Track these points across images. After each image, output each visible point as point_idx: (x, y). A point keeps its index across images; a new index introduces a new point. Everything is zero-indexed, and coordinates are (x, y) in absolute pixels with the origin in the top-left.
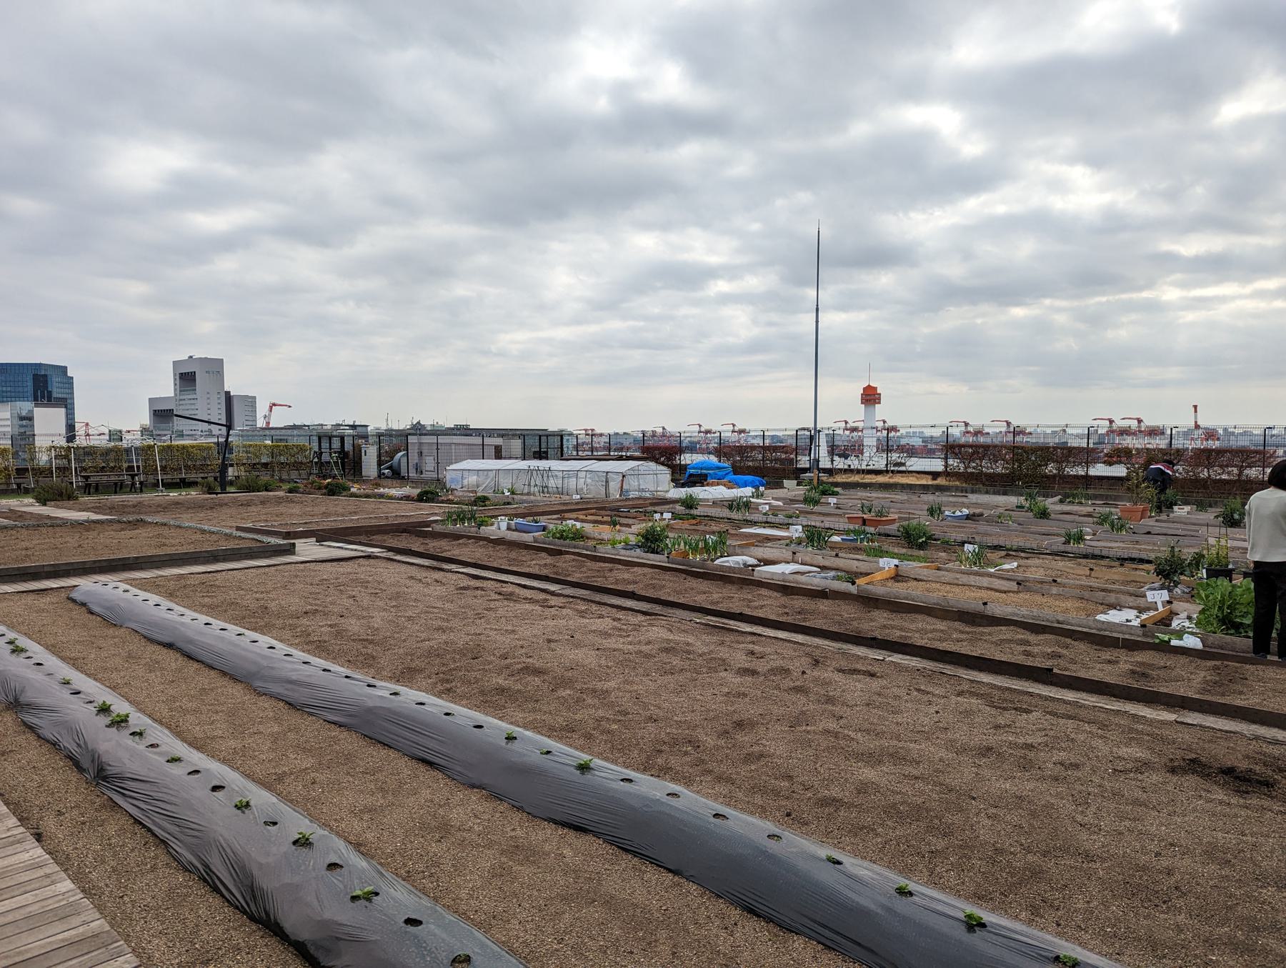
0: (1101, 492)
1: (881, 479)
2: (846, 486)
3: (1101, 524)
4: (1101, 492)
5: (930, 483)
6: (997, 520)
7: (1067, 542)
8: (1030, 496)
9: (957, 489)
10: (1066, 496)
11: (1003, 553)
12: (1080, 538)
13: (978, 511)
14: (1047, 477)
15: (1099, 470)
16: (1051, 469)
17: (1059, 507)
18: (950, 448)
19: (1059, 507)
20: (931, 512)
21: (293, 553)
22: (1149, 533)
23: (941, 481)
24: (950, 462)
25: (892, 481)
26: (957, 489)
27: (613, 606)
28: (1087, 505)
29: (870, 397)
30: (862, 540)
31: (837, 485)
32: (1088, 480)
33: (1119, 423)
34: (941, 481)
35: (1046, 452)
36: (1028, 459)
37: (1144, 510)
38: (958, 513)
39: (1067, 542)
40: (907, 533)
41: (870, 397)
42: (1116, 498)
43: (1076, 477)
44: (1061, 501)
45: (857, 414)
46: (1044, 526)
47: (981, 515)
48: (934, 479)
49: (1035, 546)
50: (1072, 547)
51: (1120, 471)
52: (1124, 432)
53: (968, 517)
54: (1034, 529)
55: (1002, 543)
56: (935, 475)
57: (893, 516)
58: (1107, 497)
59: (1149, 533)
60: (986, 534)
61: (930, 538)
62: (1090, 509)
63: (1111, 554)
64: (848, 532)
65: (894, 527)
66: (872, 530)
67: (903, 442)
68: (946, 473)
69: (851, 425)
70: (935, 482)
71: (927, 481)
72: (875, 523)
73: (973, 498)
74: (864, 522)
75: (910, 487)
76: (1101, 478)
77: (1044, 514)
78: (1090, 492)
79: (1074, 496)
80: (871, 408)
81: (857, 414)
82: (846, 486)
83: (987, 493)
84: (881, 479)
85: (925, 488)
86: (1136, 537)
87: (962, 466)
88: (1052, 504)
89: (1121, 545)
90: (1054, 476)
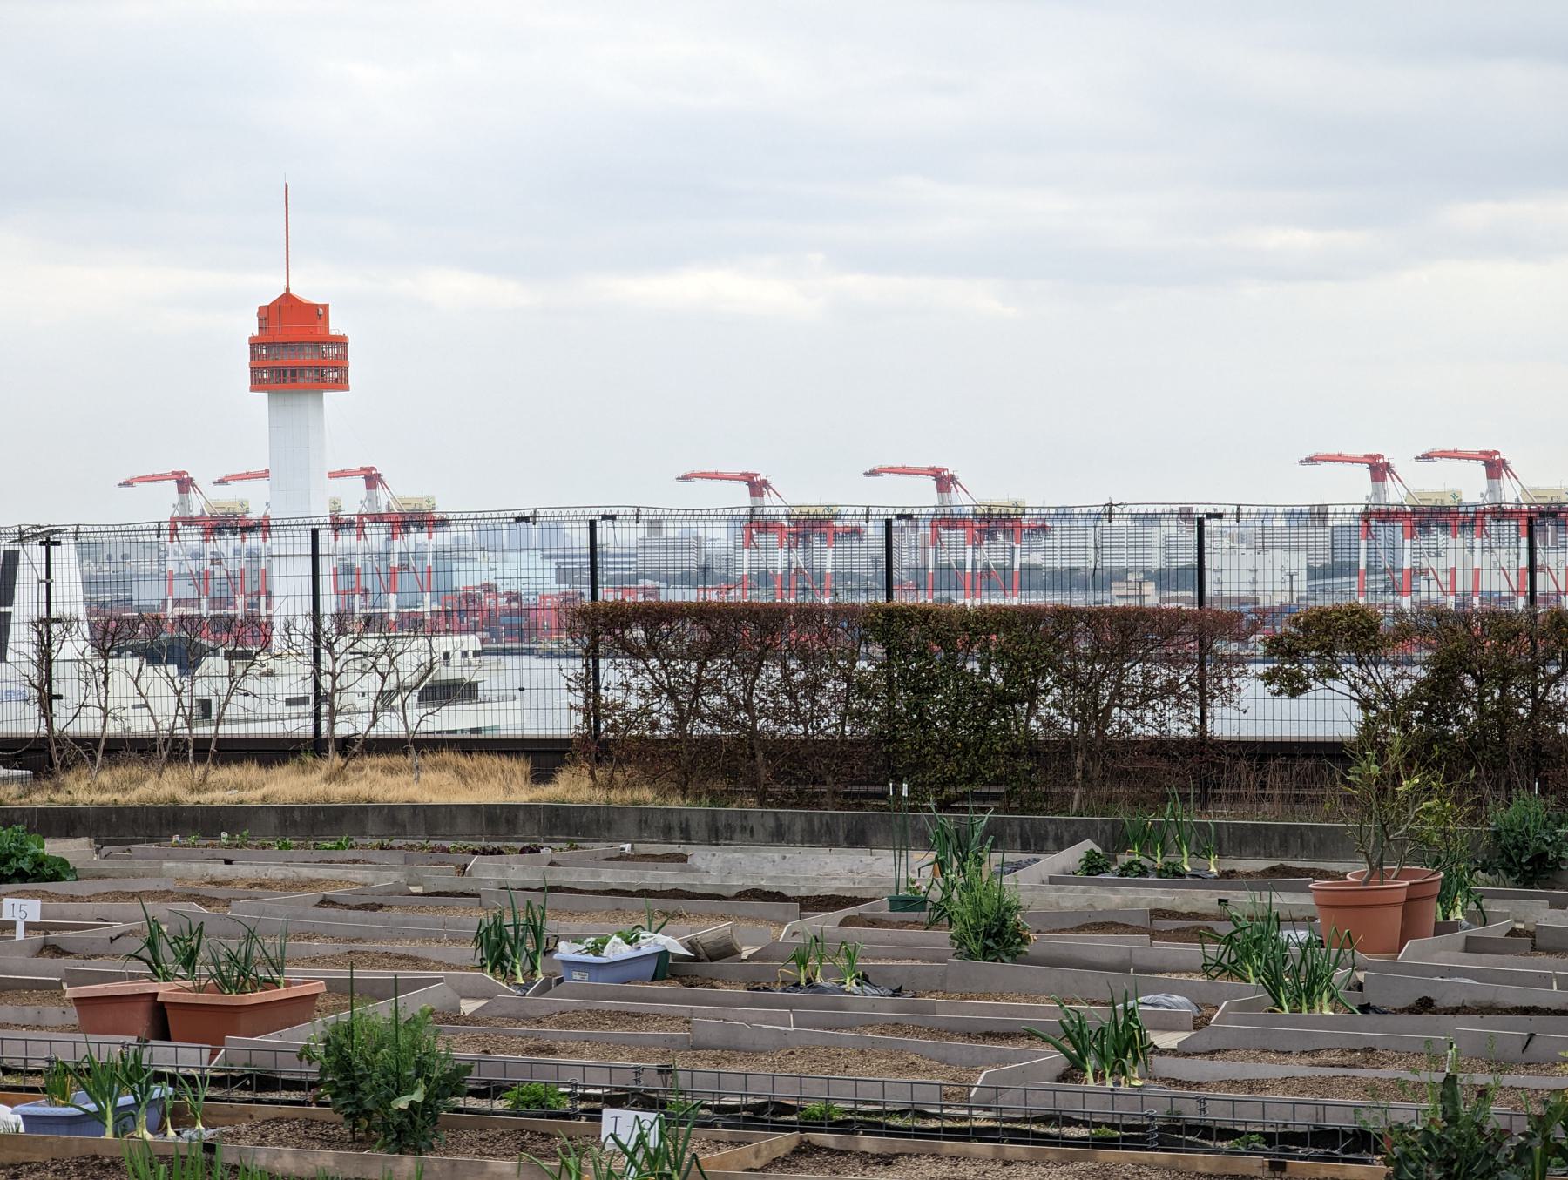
0: (1268, 816)
1: (289, 785)
2: (116, 827)
3: (1232, 970)
4: (1268, 816)
5: (523, 794)
6: (785, 979)
7: (1072, 1072)
8: (956, 848)
9: (645, 822)
10: (1117, 840)
11: (784, 1142)
12: (1126, 1045)
13: (710, 931)
14: (1034, 749)
15: (1253, 711)
16: (1050, 713)
17: (1076, 898)
18: (600, 627)
19: (1076, 898)
20: (496, 949)
21: (209, 702)
22: (1424, 1005)
23: (572, 787)
24: (612, 674)
25: (340, 792)
26: (645, 822)
27: (272, 1102)
28: (1199, 879)
29: (296, 352)
30: (125, 1119)
31: (68, 822)
32: (1213, 765)
33: (1416, 483)
34: (572, 787)
35: (1033, 640)
36: (952, 668)
37: (1413, 899)
38: (617, 950)
39: (1072, 1072)
40: (344, 1066)
41: (296, 352)
42: (1325, 843)
43: (1161, 747)
44: (1093, 867)
45: (233, 436)
46: (1008, 995)
47: (726, 951)
48: (541, 776)
49: (927, 1098)
50: (1096, 1093)
51: (1327, 712)
52: (1431, 518)
53: (664, 967)
54: (948, 1008)
55: (786, 1092)
56: (543, 756)
57: (302, 980)
58: (1286, 840)
59: (1424, 1005)
60: (730, 1049)
61: (453, 1083)
62: (1203, 900)
63: (1250, 1118)
64: (56, 1078)
65: (308, 1033)
66: (187, 1057)
67: (467, 577)
68: (599, 745)
69: (207, 499)
70: (545, 793)
71: (503, 786)
72: (209, 1023)
73: (714, 865)
74: (162, 1021)
75: (429, 822)
76: (1262, 753)
77: (997, 936)
78: (1220, 816)
79: (1147, 839)
80: (300, 408)
81: (233, 436)
82: (116, 827)
83: (779, 836)
84: (289, 785)
85: (497, 824)
86: (1370, 1030)
87: (663, 709)
88: (1038, 882)
89: (1298, 1068)
90: (1065, 749)
